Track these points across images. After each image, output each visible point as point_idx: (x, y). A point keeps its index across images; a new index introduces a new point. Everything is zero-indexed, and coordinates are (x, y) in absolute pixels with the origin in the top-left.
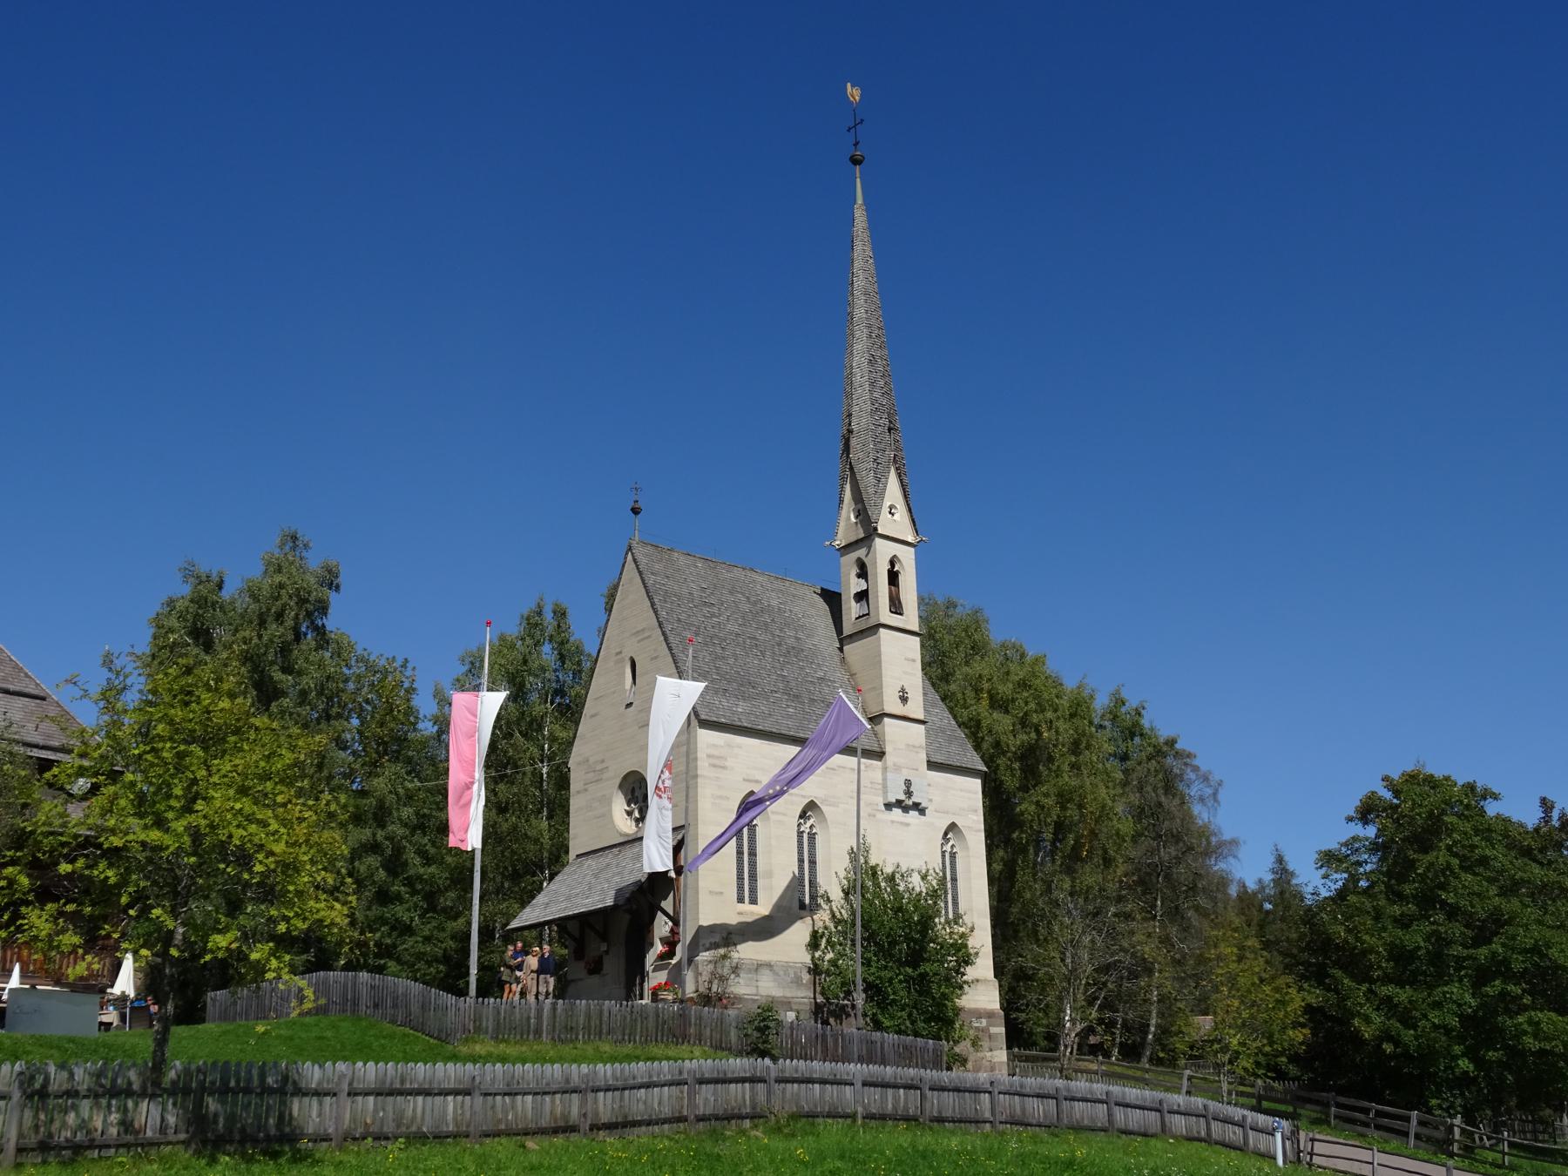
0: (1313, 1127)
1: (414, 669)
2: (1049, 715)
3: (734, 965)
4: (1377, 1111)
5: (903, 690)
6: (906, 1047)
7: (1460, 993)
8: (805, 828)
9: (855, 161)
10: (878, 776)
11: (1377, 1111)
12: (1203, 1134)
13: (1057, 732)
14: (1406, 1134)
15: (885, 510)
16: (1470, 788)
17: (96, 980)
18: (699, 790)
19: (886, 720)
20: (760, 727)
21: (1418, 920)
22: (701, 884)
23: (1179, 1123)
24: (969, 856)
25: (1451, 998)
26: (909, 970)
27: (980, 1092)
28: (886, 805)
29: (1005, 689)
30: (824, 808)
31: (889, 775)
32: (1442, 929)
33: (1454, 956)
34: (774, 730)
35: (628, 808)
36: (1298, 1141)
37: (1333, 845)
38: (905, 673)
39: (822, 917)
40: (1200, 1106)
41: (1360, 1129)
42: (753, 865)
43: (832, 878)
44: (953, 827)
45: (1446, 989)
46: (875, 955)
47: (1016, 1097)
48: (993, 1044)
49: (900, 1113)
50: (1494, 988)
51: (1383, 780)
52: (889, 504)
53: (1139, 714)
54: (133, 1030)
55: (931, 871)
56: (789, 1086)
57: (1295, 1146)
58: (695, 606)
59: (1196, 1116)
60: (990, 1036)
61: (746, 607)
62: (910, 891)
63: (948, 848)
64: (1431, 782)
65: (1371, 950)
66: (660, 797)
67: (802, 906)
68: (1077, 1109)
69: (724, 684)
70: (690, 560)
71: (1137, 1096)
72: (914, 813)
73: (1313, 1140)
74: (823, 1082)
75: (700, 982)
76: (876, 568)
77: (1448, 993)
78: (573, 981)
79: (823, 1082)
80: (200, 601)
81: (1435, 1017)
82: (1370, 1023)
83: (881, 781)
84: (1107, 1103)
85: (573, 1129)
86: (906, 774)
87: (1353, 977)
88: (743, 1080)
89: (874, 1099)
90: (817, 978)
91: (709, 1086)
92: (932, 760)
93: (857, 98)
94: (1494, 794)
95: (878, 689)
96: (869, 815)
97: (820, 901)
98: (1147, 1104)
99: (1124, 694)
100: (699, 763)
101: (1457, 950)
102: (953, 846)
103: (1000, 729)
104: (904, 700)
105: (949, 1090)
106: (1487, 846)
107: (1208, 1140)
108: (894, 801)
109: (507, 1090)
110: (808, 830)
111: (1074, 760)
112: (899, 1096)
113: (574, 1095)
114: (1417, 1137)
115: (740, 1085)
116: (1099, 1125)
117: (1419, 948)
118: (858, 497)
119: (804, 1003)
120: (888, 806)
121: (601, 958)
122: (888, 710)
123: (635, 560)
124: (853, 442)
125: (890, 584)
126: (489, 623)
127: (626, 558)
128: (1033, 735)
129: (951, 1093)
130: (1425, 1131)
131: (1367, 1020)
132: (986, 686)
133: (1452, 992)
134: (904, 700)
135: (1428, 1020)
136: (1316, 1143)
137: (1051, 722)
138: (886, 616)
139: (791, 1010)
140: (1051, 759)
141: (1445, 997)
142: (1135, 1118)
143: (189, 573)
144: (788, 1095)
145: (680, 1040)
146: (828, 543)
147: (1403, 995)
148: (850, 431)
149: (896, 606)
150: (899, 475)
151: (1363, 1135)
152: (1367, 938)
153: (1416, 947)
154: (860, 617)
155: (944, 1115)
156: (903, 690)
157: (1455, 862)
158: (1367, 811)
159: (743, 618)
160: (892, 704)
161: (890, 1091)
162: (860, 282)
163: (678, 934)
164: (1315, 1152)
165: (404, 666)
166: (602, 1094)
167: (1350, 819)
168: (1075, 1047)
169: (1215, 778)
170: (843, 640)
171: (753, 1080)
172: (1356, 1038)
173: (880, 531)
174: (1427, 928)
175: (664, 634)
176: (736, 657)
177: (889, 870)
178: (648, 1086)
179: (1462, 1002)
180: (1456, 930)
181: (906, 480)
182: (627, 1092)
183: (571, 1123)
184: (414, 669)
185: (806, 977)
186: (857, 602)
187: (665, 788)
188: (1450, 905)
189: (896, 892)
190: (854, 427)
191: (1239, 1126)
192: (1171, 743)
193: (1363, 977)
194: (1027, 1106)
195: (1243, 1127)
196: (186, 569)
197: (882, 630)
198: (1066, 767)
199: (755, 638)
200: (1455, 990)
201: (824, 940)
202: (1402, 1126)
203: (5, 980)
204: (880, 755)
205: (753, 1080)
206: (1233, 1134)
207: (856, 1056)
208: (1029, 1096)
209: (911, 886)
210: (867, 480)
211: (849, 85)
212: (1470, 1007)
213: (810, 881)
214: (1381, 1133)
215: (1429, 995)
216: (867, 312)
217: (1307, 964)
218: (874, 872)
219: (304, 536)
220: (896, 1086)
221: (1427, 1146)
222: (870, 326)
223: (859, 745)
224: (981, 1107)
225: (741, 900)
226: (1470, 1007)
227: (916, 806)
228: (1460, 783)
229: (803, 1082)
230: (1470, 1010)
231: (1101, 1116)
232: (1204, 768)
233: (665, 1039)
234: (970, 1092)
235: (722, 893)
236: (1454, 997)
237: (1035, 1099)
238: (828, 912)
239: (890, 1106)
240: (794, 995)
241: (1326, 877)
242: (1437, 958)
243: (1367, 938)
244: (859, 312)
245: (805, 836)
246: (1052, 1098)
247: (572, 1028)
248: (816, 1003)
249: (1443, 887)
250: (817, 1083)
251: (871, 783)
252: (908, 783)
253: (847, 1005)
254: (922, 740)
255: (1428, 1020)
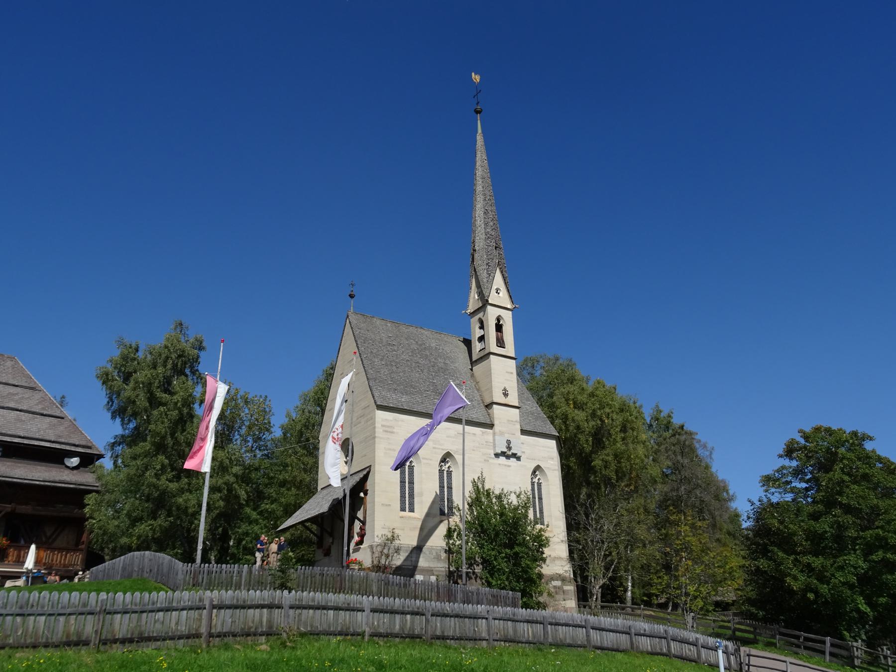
0: (766, 648)
1: (270, 401)
2: (607, 410)
3: (396, 547)
4: (804, 637)
5: (505, 389)
6: (493, 596)
7: (855, 560)
8: (445, 468)
9: (477, 112)
10: (490, 438)
11: (804, 637)
12: (665, 650)
13: (612, 420)
14: (823, 653)
15: (493, 291)
16: (855, 434)
17: (73, 567)
18: (376, 445)
19: (495, 406)
20: (415, 410)
21: (825, 515)
22: (376, 500)
23: (645, 643)
24: (548, 485)
25: (849, 564)
26: (508, 551)
27: (479, 618)
28: (495, 454)
29: (582, 398)
30: (456, 456)
31: (497, 438)
32: (840, 519)
33: (851, 537)
34: (424, 411)
35: (345, 460)
36: (740, 656)
37: (769, 471)
38: (508, 380)
39: (455, 520)
40: (662, 631)
41: (795, 649)
42: (412, 489)
43: (460, 496)
44: (538, 468)
45: (845, 558)
46: (486, 542)
47: (509, 623)
48: (566, 597)
49: (406, 632)
50: (878, 556)
51: (799, 432)
52: (495, 288)
53: (670, 416)
54: (32, 586)
55: (523, 493)
56: (305, 611)
57: (738, 659)
58: (383, 346)
59: (659, 638)
60: (564, 592)
61: (415, 347)
62: (509, 504)
63: (536, 480)
64: (829, 431)
65: (794, 534)
66: (335, 443)
67: (442, 513)
68: (560, 631)
69: (395, 386)
70: (383, 323)
71: (624, 625)
72: (513, 460)
73: (749, 655)
74: (337, 608)
75: (374, 558)
76: (488, 322)
77: (847, 560)
78: (317, 561)
79: (337, 608)
80: (125, 358)
81: (840, 577)
82: (797, 581)
83: (492, 441)
84: (586, 628)
85: (86, 643)
86: (507, 437)
87: (785, 551)
88: (262, 607)
89: (383, 622)
90: (451, 555)
91: (227, 611)
92: (524, 429)
93: (478, 80)
94: (869, 436)
95: (490, 389)
96: (485, 460)
97: (454, 510)
98: (620, 629)
99: (661, 408)
100: (376, 430)
101: (852, 533)
102: (539, 479)
103: (579, 419)
104: (506, 395)
105: (451, 616)
106: (866, 468)
107: (668, 655)
108: (500, 452)
109: (18, 611)
110: (446, 469)
111: (623, 435)
112: (406, 620)
113: (89, 617)
114: (831, 654)
115: (258, 611)
116: (579, 643)
117: (826, 532)
118: (479, 286)
119: (442, 571)
120: (497, 455)
121: (330, 546)
122: (495, 400)
123: (350, 322)
124: (476, 256)
125: (496, 331)
126: (223, 341)
127: (346, 322)
128: (599, 422)
129: (453, 619)
130: (836, 650)
131: (795, 578)
132: (571, 397)
133: (850, 560)
134: (506, 395)
135: (836, 578)
136: (751, 657)
137: (608, 414)
138: (494, 348)
139: (433, 575)
140: (610, 435)
141: (845, 563)
142: (610, 639)
143: (121, 343)
144: (303, 618)
145: (338, 591)
146: (464, 312)
147: (817, 562)
148: (475, 250)
149: (501, 343)
150: (502, 272)
151: (797, 653)
152: (791, 526)
153: (824, 531)
154: (481, 350)
155: (446, 634)
156: (505, 389)
157: (846, 478)
158: (789, 452)
159: (412, 352)
160: (498, 397)
161: (398, 617)
162: (479, 172)
163: (364, 530)
164: (751, 663)
165: (265, 400)
166: (119, 616)
167: (781, 456)
168: (599, 595)
169: (709, 446)
170: (473, 363)
171: (270, 607)
172: (791, 592)
173: (490, 302)
174: (830, 519)
175: (362, 360)
176: (404, 372)
177: (497, 492)
178: (167, 610)
179: (857, 566)
180: (849, 519)
181: (506, 275)
182: (145, 615)
183: (84, 638)
184: (270, 401)
185: (444, 555)
186: (479, 342)
187: (338, 438)
188: (845, 504)
189: (502, 506)
190: (477, 248)
191: (693, 645)
192: (682, 427)
193: (791, 550)
194: (518, 629)
195: (696, 646)
196: (118, 341)
197: (491, 356)
198: (618, 439)
199: (418, 362)
200: (852, 558)
201: (456, 533)
202: (821, 647)
203: (20, 567)
204: (491, 426)
205: (270, 607)
206: (689, 651)
207: (375, 589)
208: (521, 622)
209: (510, 501)
210: (483, 275)
211: (473, 74)
212: (863, 569)
213: (448, 499)
214: (808, 652)
215: (835, 562)
216: (483, 187)
217: (757, 544)
218: (488, 494)
219: (186, 323)
220: (403, 613)
221: (838, 661)
222: (485, 195)
223: (462, 414)
224: (478, 629)
225: (403, 509)
226: (863, 569)
227: (514, 455)
228: (848, 432)
229: (319, 609)
230: (863, 571)
231: (581, 636)
232: (703, 440)
233: (327, 590)
234: (470, 618)
235: (390, 505)
236: (851, 563)
237: (525, 624)
238: (459, 517)
239: (397, 627)
240: (435, 566)
241: (766, 491)
242: (839, 538)
243: (791, 526)
244: (479, 188)
245: (445, 472)
246: (541, 623)
247: (262, 583)
248: (449, 570)
249: (840, 493)
250: (331, 609)
251: (486, 442)
252: (509, 442)
253: (470, 572)
254: (518, 418)
255: (836, 578)
